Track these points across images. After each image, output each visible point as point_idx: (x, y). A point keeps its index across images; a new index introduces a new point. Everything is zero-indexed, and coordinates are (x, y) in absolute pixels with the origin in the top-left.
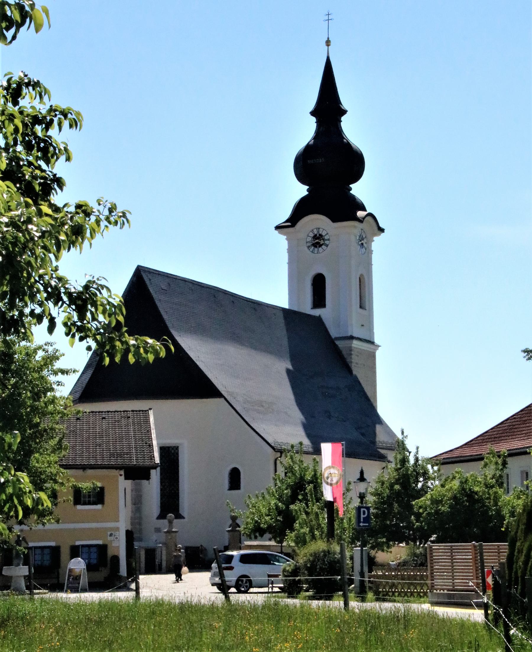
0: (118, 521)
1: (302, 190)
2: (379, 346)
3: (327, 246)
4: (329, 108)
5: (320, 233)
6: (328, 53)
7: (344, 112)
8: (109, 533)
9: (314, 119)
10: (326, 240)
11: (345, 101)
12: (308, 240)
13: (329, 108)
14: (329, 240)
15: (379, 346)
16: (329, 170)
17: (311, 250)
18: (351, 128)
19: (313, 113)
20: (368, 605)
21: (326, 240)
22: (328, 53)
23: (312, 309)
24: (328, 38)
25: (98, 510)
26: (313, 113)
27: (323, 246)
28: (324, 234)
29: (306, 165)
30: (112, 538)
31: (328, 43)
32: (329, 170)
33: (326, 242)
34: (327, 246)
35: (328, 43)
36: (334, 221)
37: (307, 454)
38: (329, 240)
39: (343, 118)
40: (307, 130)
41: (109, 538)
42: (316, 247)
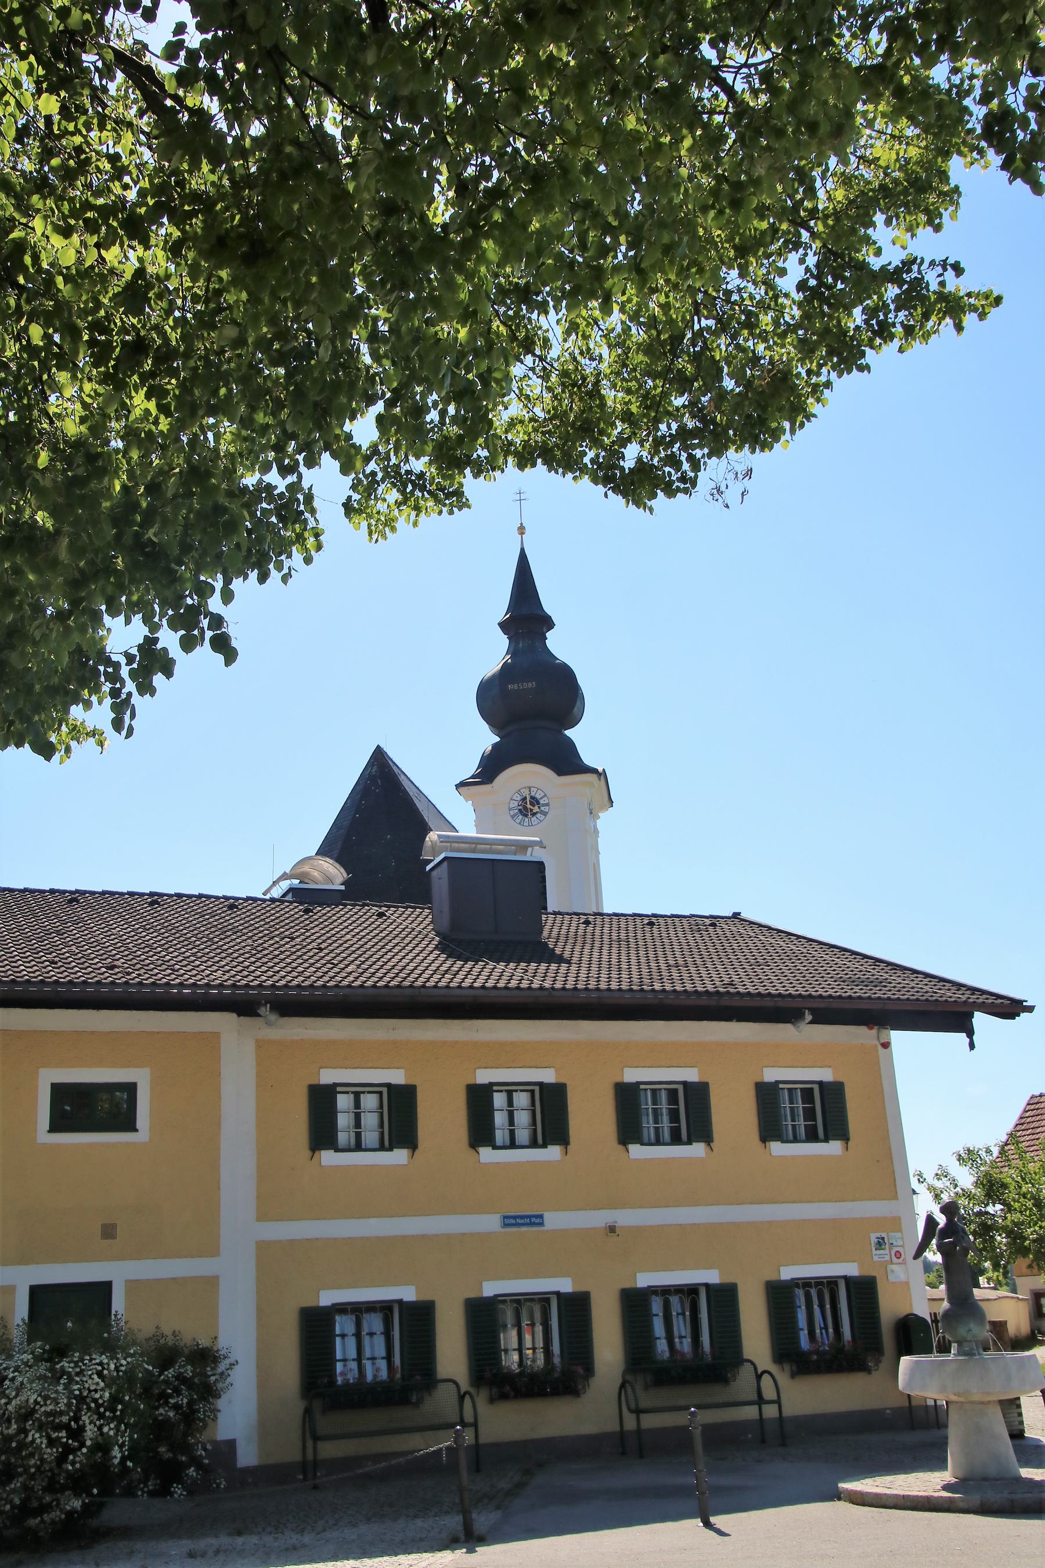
0: (263, 1248)
3: (545, 814)
4: (526, 618)
5: (533, 794)
8: (873, 1237)
10: (544, 805)
12: (512, 806)
13: (526, 618)
14: (547, 805)
17: (518, 821)
21: (544, 805)
23: (49, 1131)
25: (691, 1161)
26: (504, 626)
27: (538, 815)
28: (538, 796)
29: (496, 699)
30: (885, 1254)
31: (522, 530)
33: (542, 808)
34: (545, 814)
35: (522, 530)
36: (559, 775)
38: (547, 805)
40: (493, 652)
41: (877, 1255)
42: (526, 816)
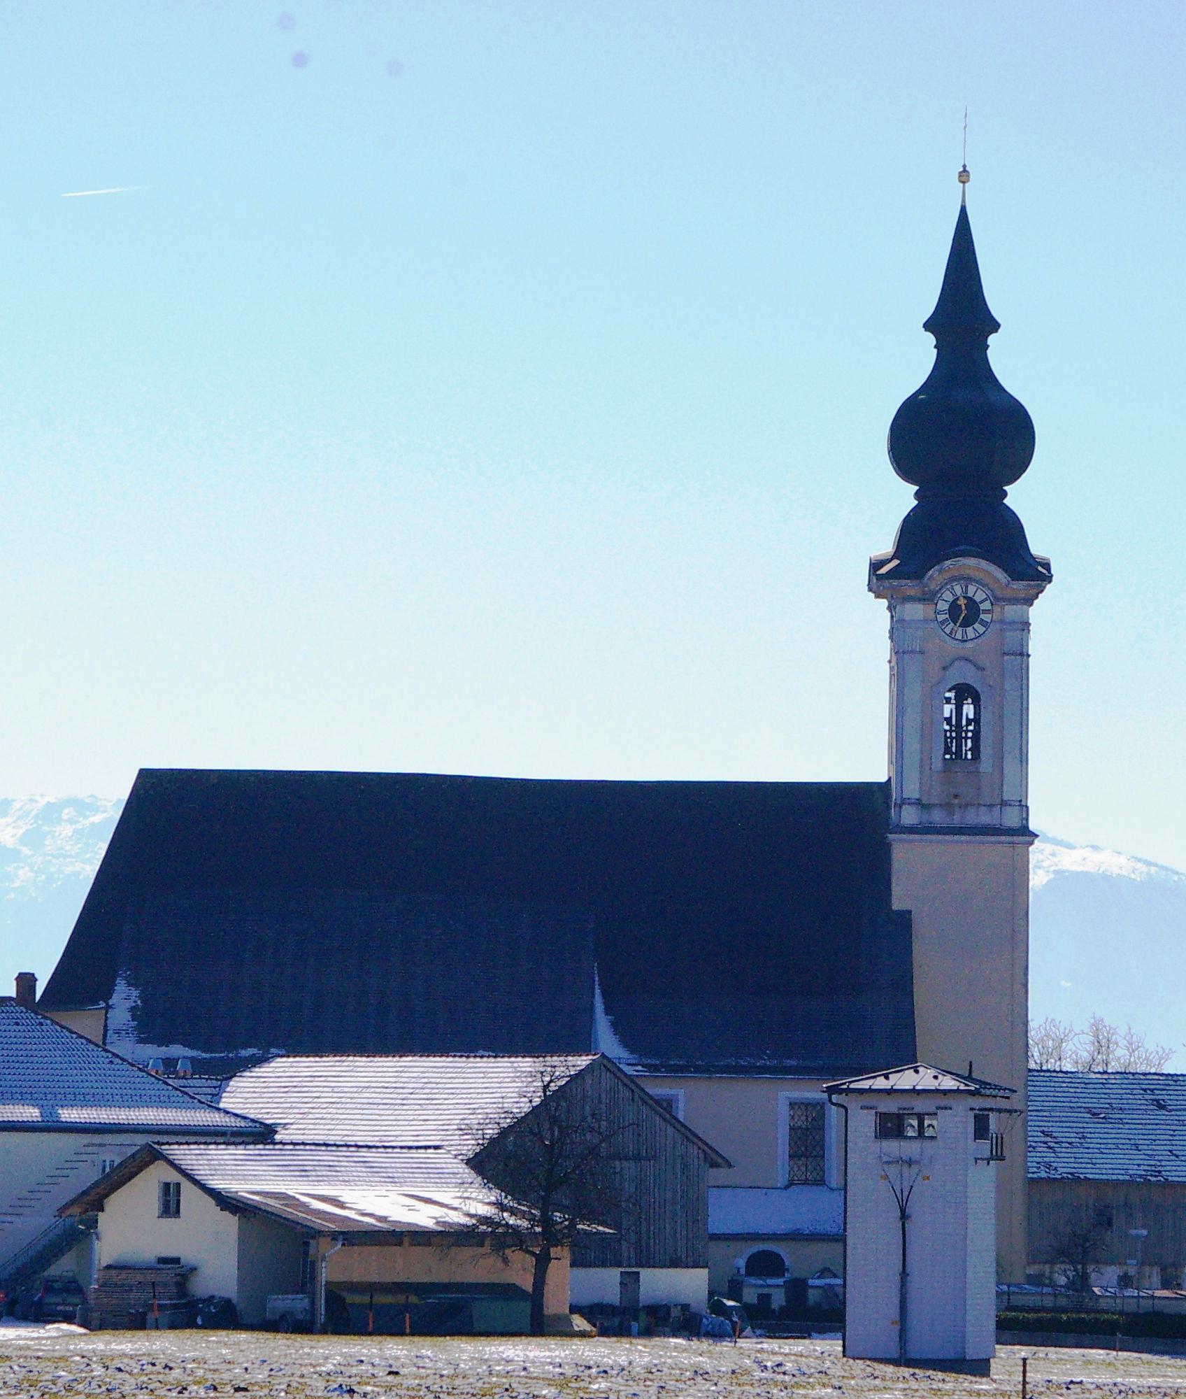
1: (885, 602)
2: (1037, 836)
4: (962, 316)
6: (964, 201)
7: (995, 326)
9: (931, 339)
11: (996, 298)
13: (962, 316)
15: (1037, 836)
16: (961, 445)
18: (1008, 360)
19: (928, 326)
20: (92, 819)
22: (964, 201)
24: (964, 166)
26: (928, 326)
31: (964, 176)
32: (961, 445)
35: (964, 176)
37: (751, 1240)
39: (992, 340)
40: (916, 360)
